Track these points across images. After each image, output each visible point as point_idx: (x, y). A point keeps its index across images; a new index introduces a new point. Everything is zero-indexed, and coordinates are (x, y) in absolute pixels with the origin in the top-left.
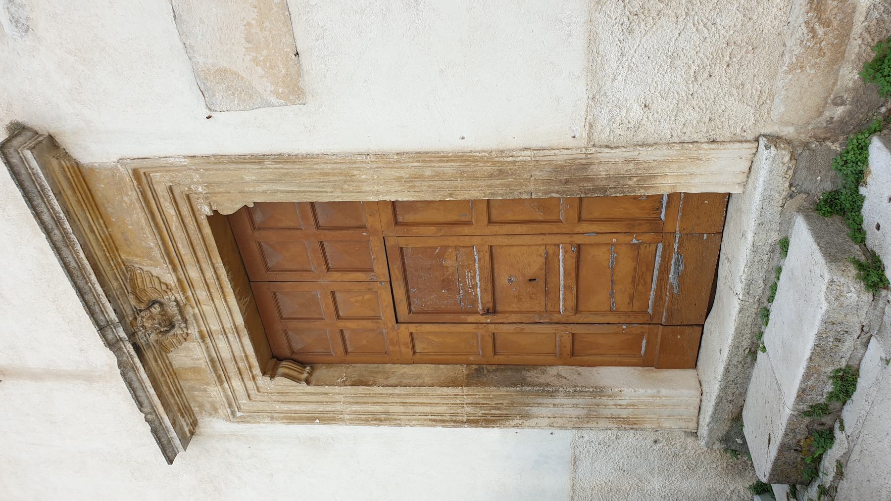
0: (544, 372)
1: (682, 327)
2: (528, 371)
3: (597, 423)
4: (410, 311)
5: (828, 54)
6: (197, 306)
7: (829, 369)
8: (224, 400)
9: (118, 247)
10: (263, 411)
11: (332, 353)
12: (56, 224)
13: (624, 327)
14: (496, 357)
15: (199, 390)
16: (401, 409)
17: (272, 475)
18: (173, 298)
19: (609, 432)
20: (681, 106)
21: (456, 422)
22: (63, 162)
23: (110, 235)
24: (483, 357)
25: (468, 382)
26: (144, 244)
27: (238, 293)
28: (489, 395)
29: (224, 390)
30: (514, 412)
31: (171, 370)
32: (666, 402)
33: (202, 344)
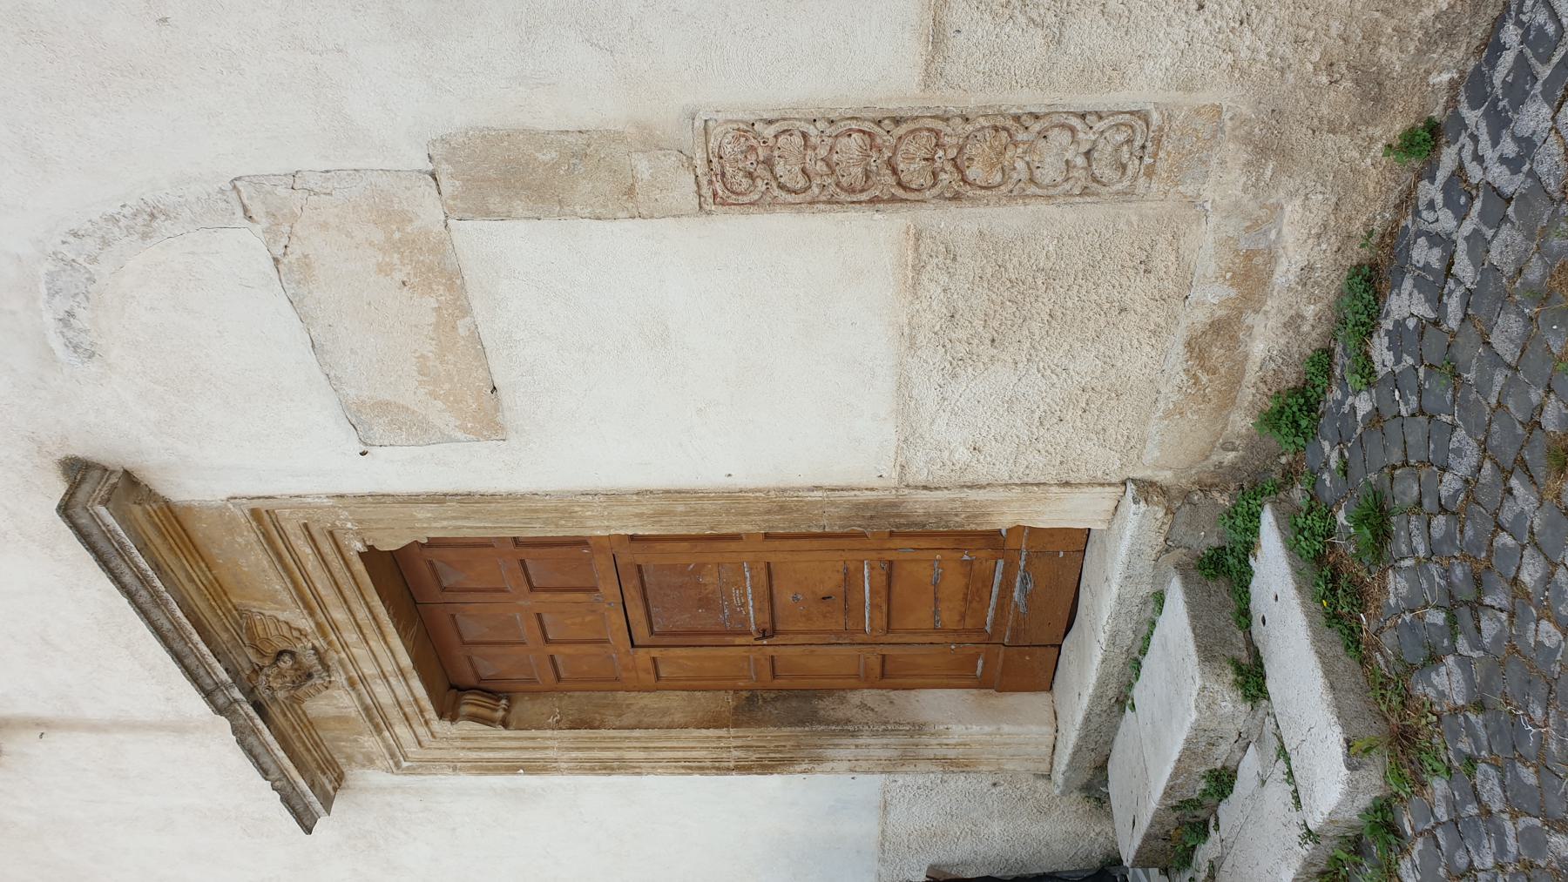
0: (843, 701)
1: (1032, 648)
2: (821, 698)
3: (915, 766)
4: (652, 632)
5: (1215, 400)
6: (344, 650)
7: (1203, 769)
8: (384, 750)
9: (227, 590)
10: (439, 760)
11: (538, 679)
12: (142, 583)
13: (953, 647)
14: (776, 681)
15: (346, 740)
16: (642, 755)
17: (454, 829)
18: (310, 645)
19: (932, 775)
20: (1022, 448)
21: (720, 769)
22: (148, 507)
23: (215, 579)
24: (757, 681)
25: (736, 719)
26: (266, 587)
27: (394, 615)
28: (766, 737)
29: (384, 740)
30: (801, 755)
31: (305, 720)
32: (1008, 741)
33: (352, 693)
